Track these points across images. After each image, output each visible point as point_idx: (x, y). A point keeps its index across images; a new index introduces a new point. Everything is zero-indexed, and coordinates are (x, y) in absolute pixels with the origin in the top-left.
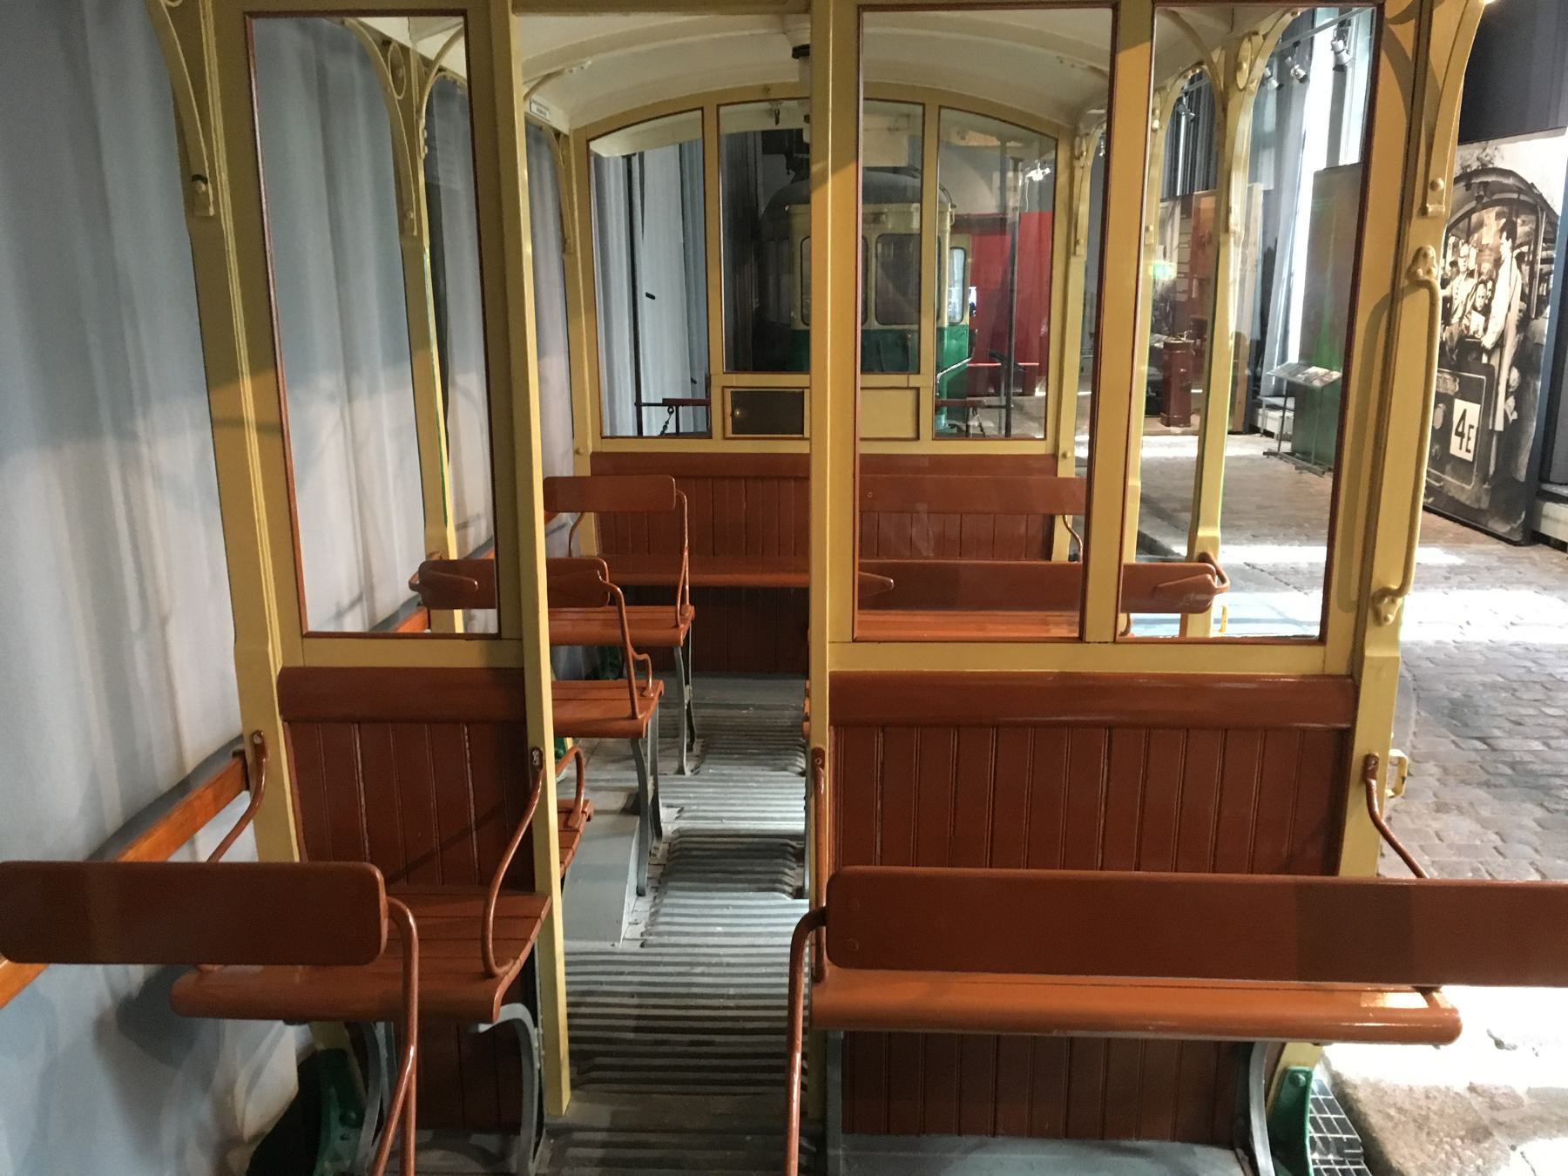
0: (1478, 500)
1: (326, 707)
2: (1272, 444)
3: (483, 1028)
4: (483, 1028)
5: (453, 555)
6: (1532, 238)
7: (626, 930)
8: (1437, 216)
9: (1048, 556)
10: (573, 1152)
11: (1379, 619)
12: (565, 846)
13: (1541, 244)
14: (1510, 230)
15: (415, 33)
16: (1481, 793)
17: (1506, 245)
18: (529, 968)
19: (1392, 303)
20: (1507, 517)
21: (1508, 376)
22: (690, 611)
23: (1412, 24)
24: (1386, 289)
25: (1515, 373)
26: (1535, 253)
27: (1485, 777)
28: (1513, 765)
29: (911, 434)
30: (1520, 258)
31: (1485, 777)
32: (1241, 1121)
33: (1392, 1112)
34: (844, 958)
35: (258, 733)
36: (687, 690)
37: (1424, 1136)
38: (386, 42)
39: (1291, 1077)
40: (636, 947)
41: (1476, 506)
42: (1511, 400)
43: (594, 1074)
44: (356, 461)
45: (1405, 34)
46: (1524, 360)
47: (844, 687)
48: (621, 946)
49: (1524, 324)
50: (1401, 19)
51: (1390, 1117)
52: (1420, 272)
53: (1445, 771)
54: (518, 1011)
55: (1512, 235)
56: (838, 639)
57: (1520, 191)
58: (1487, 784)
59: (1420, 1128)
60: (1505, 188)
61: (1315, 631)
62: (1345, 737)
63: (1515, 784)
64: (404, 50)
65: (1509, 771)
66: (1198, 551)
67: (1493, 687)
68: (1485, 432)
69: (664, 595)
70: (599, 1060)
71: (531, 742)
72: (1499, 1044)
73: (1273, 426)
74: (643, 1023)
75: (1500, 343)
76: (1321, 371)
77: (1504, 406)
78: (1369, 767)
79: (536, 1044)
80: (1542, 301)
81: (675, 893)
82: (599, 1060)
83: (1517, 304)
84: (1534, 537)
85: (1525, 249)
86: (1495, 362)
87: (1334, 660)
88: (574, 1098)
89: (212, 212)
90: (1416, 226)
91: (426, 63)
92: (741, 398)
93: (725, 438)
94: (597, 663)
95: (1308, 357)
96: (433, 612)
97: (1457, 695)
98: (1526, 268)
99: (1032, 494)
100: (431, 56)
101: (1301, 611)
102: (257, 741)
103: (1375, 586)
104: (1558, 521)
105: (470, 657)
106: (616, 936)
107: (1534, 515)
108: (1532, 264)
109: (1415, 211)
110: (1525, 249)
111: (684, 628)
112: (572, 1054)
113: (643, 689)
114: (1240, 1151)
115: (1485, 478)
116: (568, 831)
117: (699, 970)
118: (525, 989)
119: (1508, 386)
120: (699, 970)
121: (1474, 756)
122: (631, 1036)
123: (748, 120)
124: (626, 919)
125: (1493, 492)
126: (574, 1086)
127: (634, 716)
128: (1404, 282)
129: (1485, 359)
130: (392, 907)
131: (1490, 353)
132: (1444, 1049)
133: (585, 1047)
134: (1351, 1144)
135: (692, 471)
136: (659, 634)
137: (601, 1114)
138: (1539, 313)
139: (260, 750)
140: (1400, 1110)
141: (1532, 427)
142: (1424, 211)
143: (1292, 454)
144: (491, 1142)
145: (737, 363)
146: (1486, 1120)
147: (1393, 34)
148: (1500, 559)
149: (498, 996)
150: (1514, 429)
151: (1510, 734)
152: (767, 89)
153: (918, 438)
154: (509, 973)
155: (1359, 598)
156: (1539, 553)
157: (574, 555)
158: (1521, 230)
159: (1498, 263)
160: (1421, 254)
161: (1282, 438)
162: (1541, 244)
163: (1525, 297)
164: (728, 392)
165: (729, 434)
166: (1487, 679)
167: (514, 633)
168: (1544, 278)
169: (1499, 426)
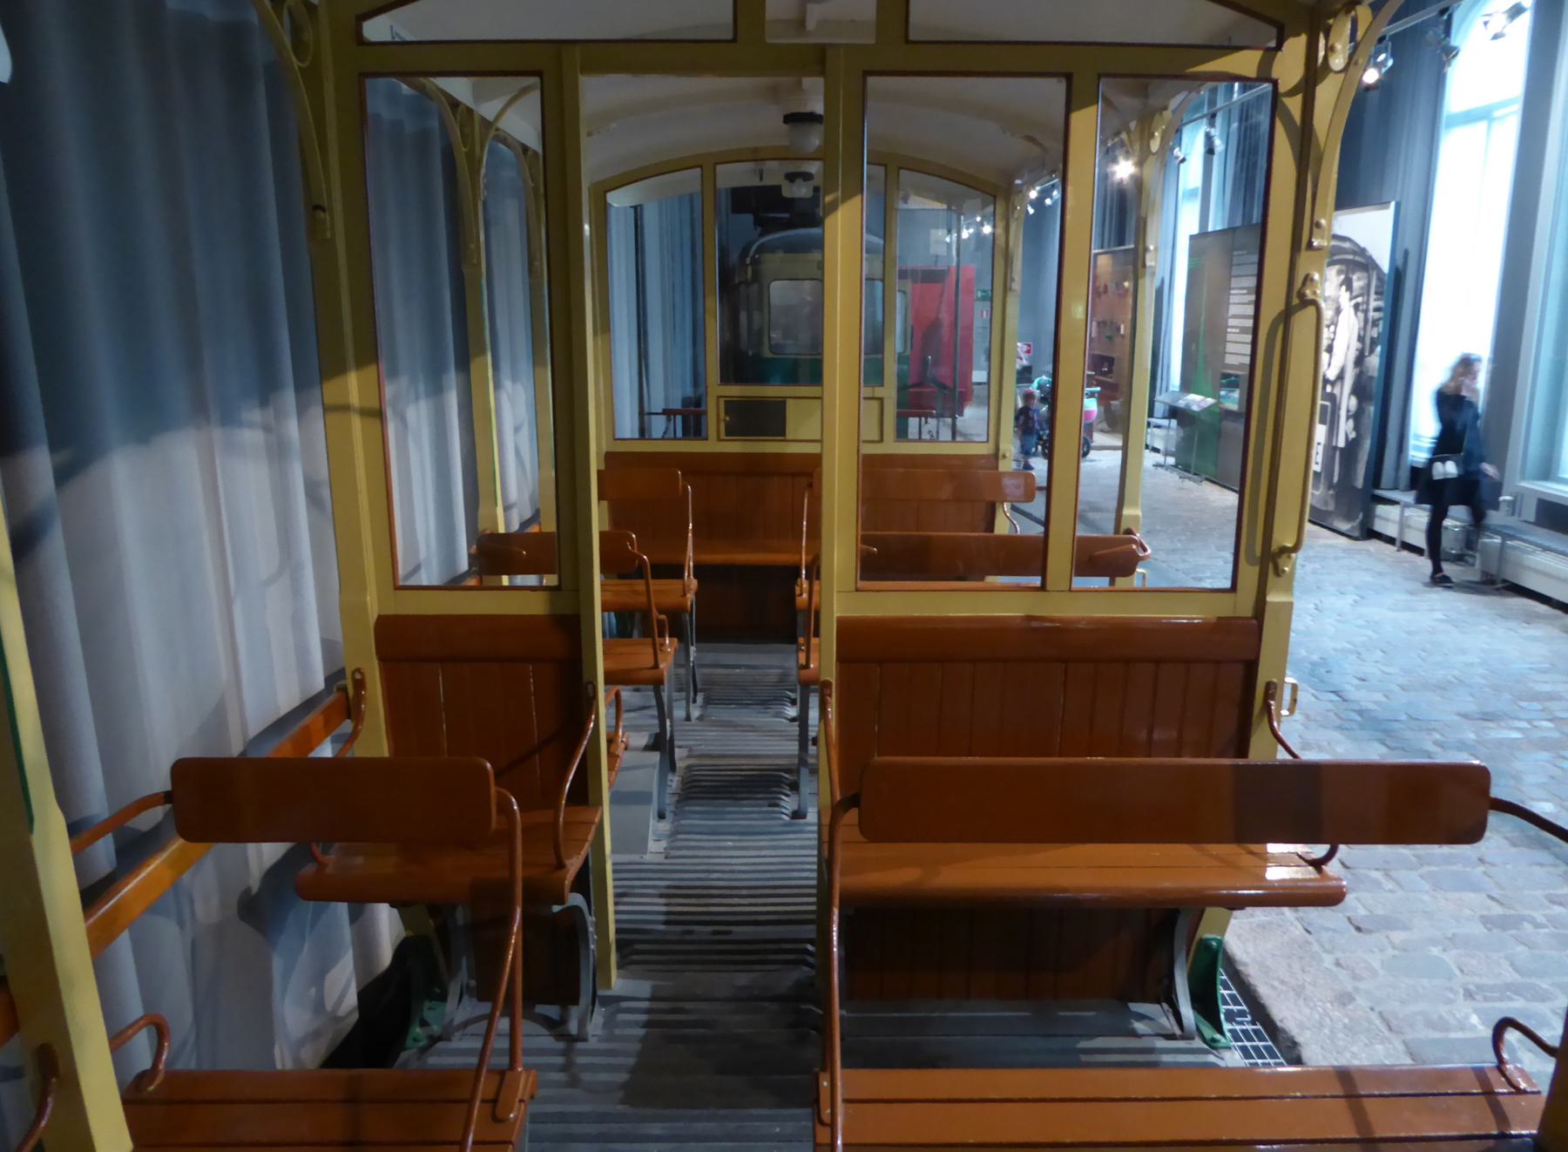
1: (412, 650)
2: (1159, 458)
3: (556, 908)
4: (556, 908)
5: (502, 530)
6: (1366, 291)
7: (653, 846)
8: (1319, 249)
10: (621, 1017)
11: (1278, 572)
12: (611, 769)
13: (1373, 296)
14: (1348, 283)
15: (479, 96)
16: (1337, 735)
17: (1344, 296)
18: (584, 871)
19: (1286, 316)
20: (1348, 518)
21: (1348, 402)
22: (694, 583)
23: (1299, 98)
24: (1281, 306)
25: (1354, 401)
26: (1368, 303)
27: (1338, 722)
28: (1360, 712)
29: (876, 437)
30: (1356, 307)
31: (1338, 722)
32: (1166, 981)
33: (1276, 983)
34: (873, 832)
35: (358, 670)
36: (693, 649)
37: (1301, 1002)
38: (455, 104)
39: (1205, 944)
40: (661, 859)
42: (1351, 422)
43: (635, 957)
45: (1294, 105)
46: (1359, 390)
47: (848, 630)
48: (648, 858)
49: (1360, 360)
50: (1292, 93)
51: (1273, 987)
52: (1308, 292)
53: (1307, 717)
54: (576, 899)
55: (1349, 288)
56: (841, 593)
57: (1354, 253)
58: (1340, 728)
59: (1298, 995)
60: (1345, 251)
61: (1227, 584)
62: (1251, 667)
63: (1362, 727)
64: (470, 111)
65: (1358, 718)
66: (1124, 526)
67: (1343, 651)
68: (1330, 449)
69: (676, 571)
70: (638, 947)
71: (586, 678)
72: (1358, 929)
73: (1159, 445)
74: (672, 917)
75: (1341, 377)
76: (1198, 398)
77: (1345, 428)
78: (1271, 691)
79: (591, 929)
80: (1374, 343)
81: (692, 810)
82: (638, 947)
83: (1355, 345)
84: (1369, 533)
85: (1359, 300)
86: (1337, 391)
87: (1243, 606)
88: (619, 976)
89: (328, 234)
90: (1304, 256)
91: (487, 124)
92: (733, 406)
93: (719, 440)
94: (628, 622)
95: (1187, 385)
97: (1315, 658)
98: (1361, 315)
99: (973, 485)
100: (490, 118)
101: (1211, 566)
102: (358, 676)
103: (1274, 547)
104: (1387, 520)
105: (536, 606)
106: (643, 849)
107: (1369, 516)
108: (1366, 312)
109: (1304, 245)
110: (1359, 300)
111: (690, 597)
112: (618, 942)
113: (663, 645)
114: (1165, 1006)
115: (1330, 486)
116: (612, 756)
117: (715, 876)
118: (582, 883)
120: (715, 876)
121: (1330, 706)
122: (662, 927)
123: (735, 175)
124: (651, 837)
125: (1337, 497)
126: (619, 967)
127: (656, 666)
128: (1296, 301)
130: (499, 793)
131: (1333, 384)
132: (1340, 906)
133: (628, 937)
134: (1242, 1014)
135: (697, 467)
136: (671, 600)
137: (643, 988)
138: (1372, 351)
139: (360, 685)
140: (1283, 982)
141: (1367, 444)
142: (1310, 244)
143: (1175, 466)
144: (552, 1011)
145: (725, 379)
146: (1349, 988)
147: (1284, 105)
148: (1344, 551)
149: (568, 883)
150: (1352, 446)
151: (1358, 688)
152: (756, 150)
153: (881, 440)
154: (573, 865)
155: (1264, 557)
156: (1374, 545)
158: (1358, 284)
159: (1338, 311)
160: (1308, 279)
161: (1167, 454)
162: (1373, 296)
163: (1361, 339)
164: (722, 401)
165: (723, 436)
166: (1338, 646)
167: (573, 589)
168: (1375, 323)
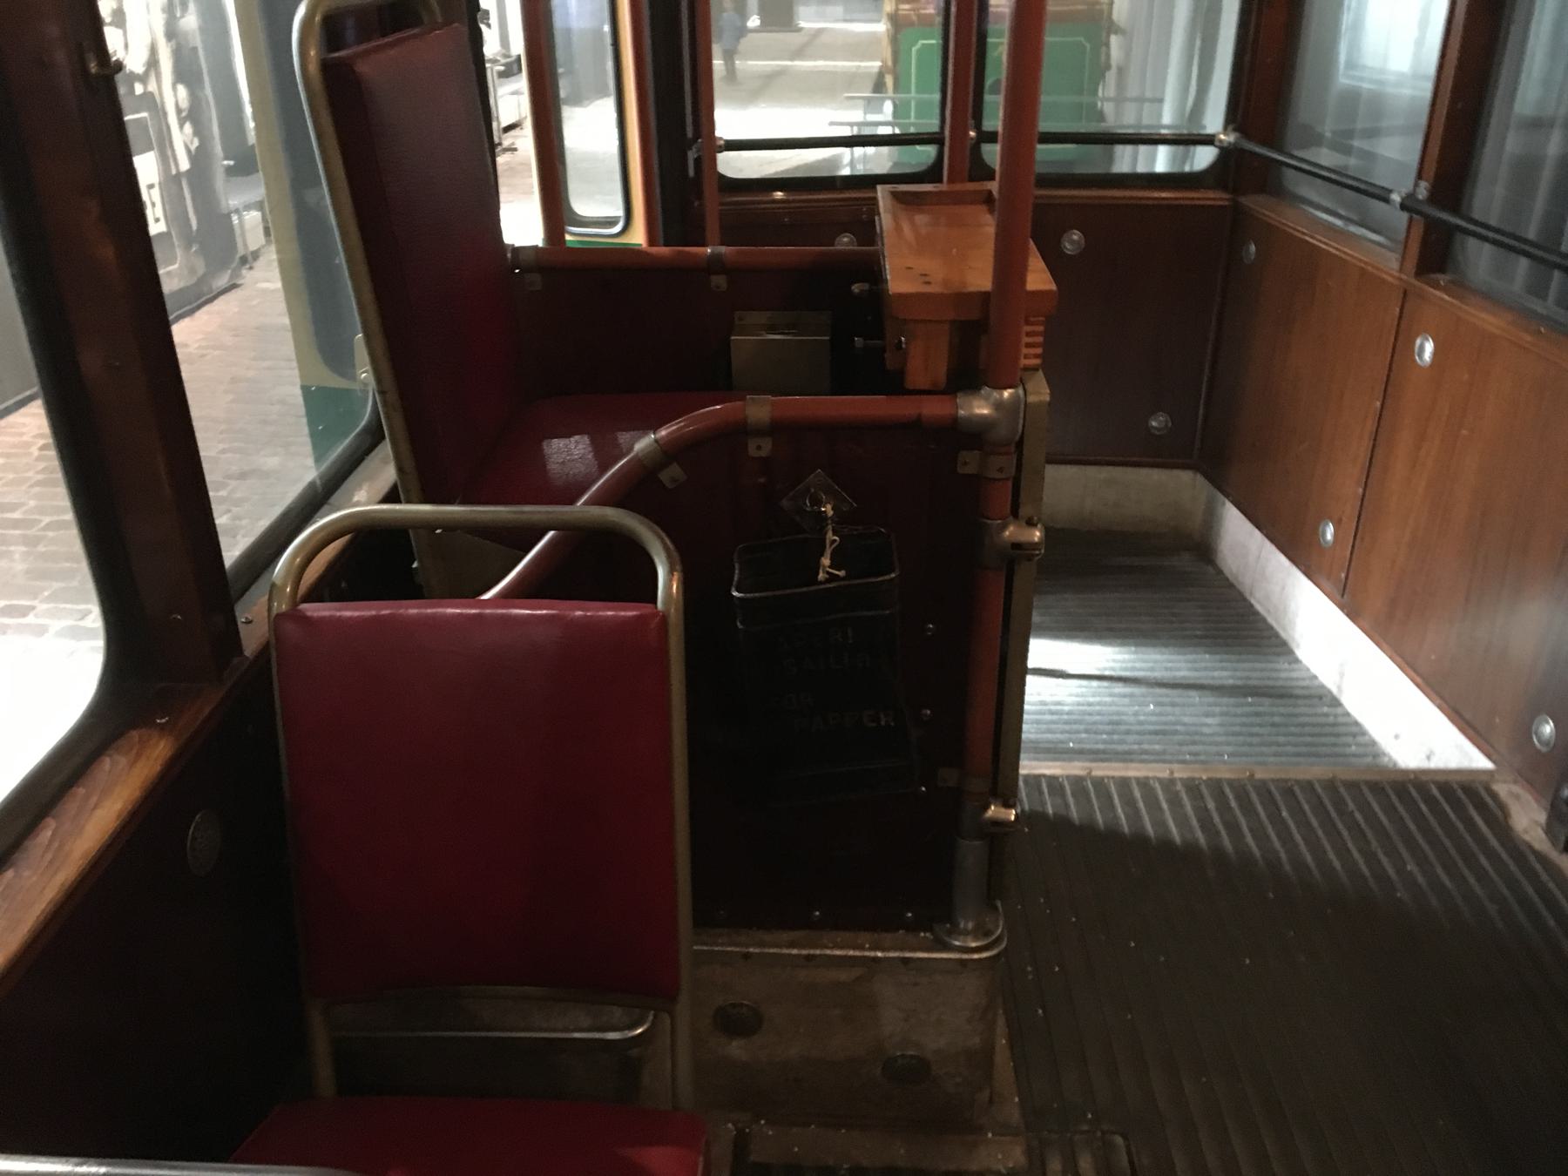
0: (192, 271)
9: (1052, 460)
21: (173, 97)
25: (182, 91)
41: (194, 280)
42: (188, 128)
44: (1048, 751)
46: (185, 73)
49: (171, 33)
75: (153, 63)
86: (152, 87)
96: (1031, 664)
119: (179, 111)
123: (1443, 279)
129: (139, 89)
131: (143, 79)
150: (200, 158)
157: (932, 124)
169: (185, 165)
